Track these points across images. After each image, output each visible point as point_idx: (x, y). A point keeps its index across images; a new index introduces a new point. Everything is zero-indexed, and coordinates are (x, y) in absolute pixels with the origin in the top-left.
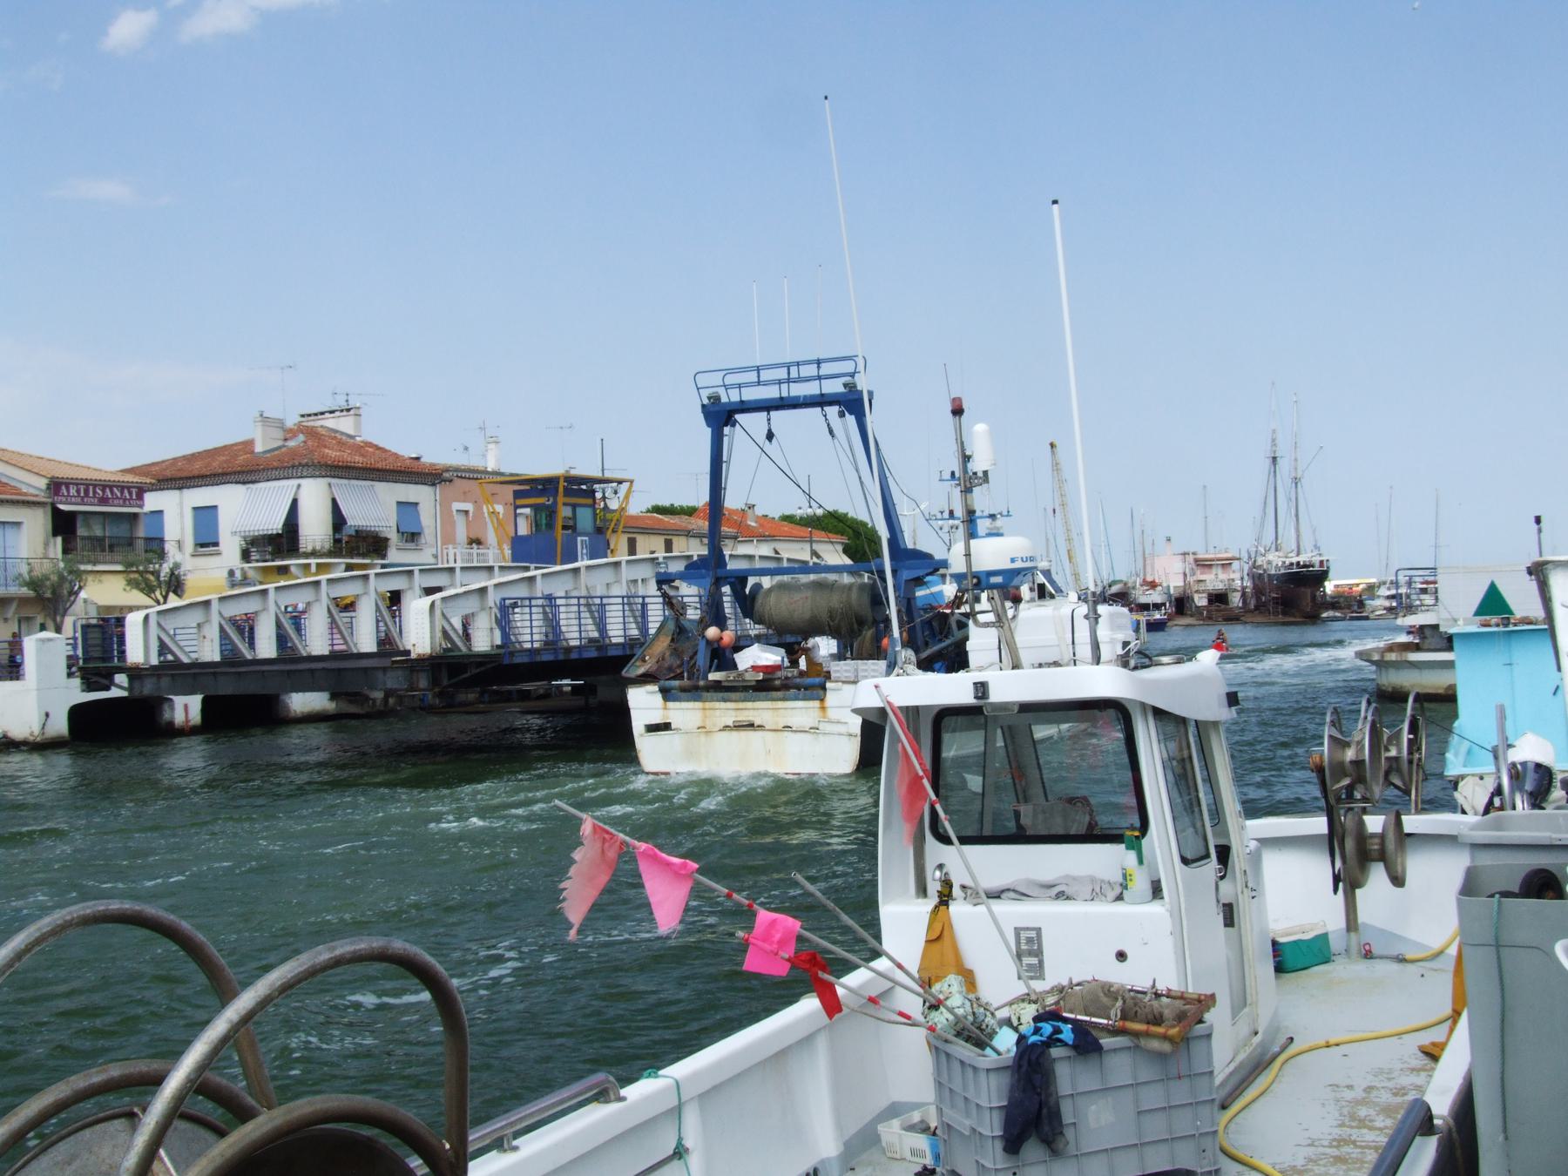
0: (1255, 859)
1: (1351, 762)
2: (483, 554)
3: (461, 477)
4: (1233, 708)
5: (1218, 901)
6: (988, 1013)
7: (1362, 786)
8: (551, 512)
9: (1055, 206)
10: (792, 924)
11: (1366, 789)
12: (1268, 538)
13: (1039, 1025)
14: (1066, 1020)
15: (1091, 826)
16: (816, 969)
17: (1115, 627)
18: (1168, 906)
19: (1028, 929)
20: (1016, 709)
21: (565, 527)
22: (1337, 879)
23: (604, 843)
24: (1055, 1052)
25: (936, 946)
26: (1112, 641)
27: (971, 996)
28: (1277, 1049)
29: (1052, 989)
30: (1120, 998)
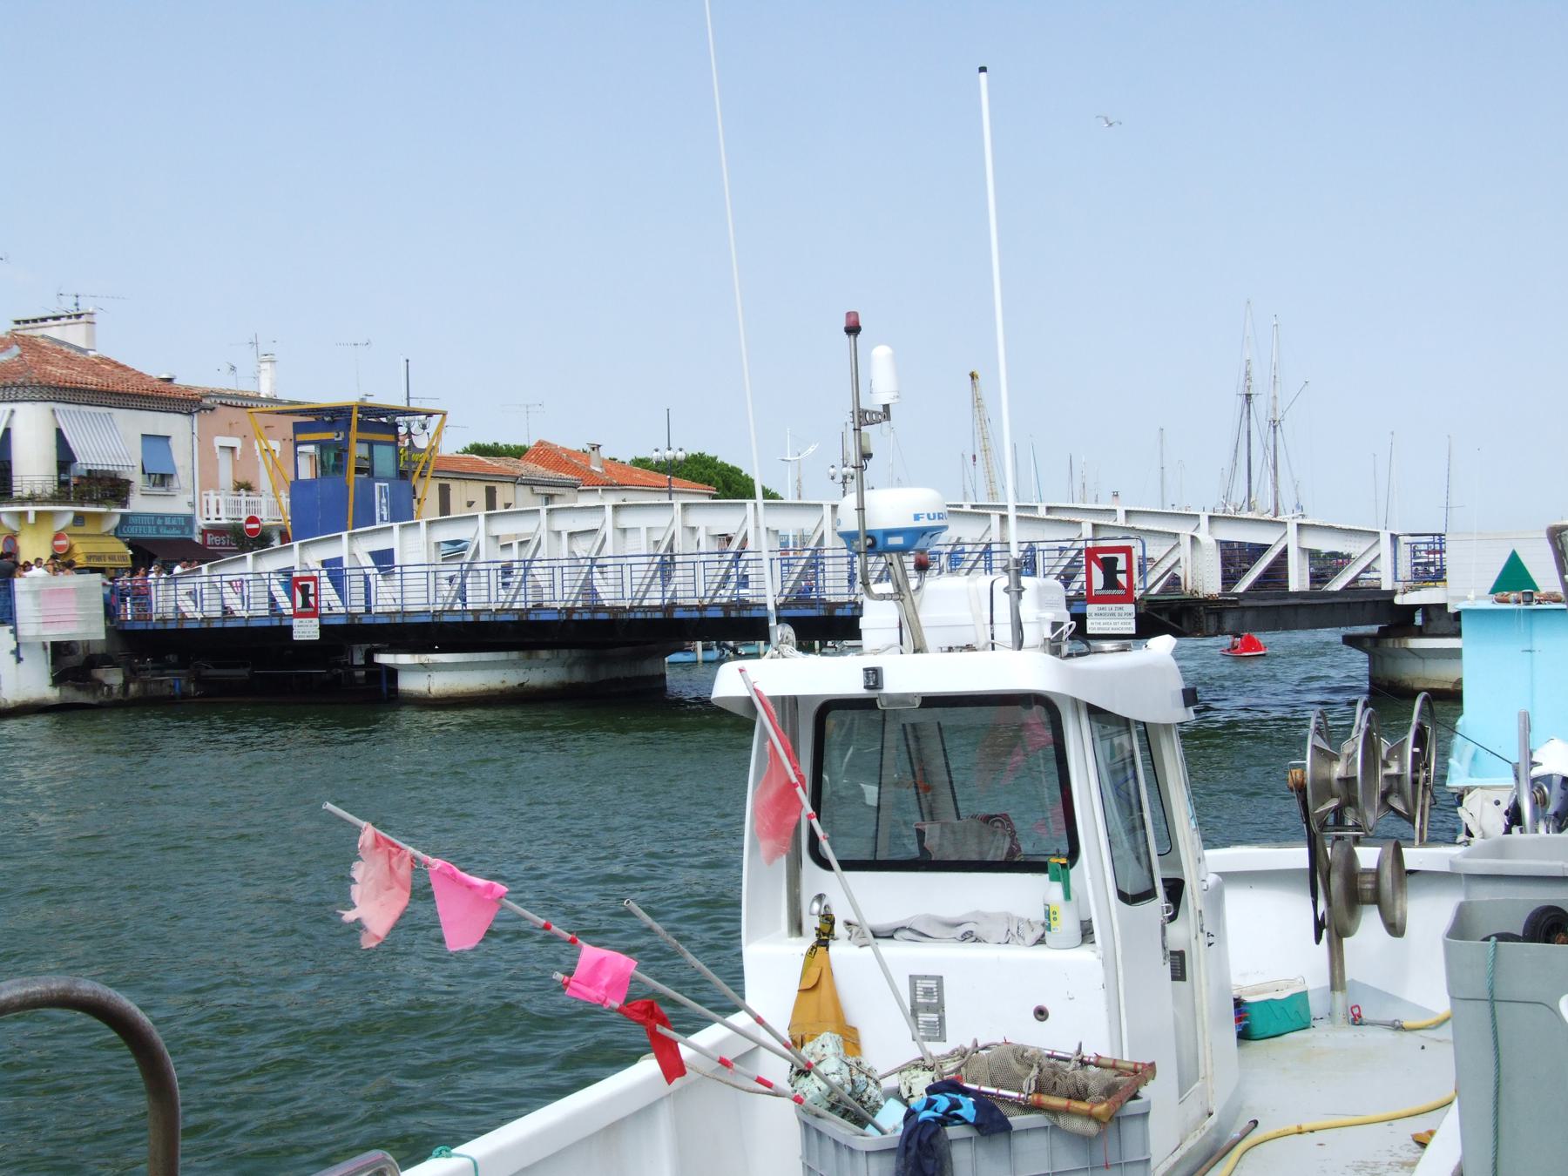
0: (1215, 898)
1: (1340, 780)
2: (254, 503)
3: (226, 405)
4: (1191, 709)
5: (1164, 948)
6: (871, 1082)
7: (1352, 810)
8: (341, 452)
9: (983, 74)
10: (626, 964)
11: (1357, 813)
12: (1240, 494)
13: (934, 1097)
14: (967, 1092)
15: (1011, 852)
16: (652, 1021)
17: (1043, 603)
18: (1100, 953)
19: (926, 977)
20: (918, 702)
21: (358, 470)
22: (1319, 926)
23: (390, 858)
24: (953, 1131)
25: (812, 996)
26: (1039, 621)
27: (851, 1060)
28: (1236, 1135)
29: (953, 1052)
30: (1035, 1065)
